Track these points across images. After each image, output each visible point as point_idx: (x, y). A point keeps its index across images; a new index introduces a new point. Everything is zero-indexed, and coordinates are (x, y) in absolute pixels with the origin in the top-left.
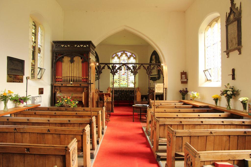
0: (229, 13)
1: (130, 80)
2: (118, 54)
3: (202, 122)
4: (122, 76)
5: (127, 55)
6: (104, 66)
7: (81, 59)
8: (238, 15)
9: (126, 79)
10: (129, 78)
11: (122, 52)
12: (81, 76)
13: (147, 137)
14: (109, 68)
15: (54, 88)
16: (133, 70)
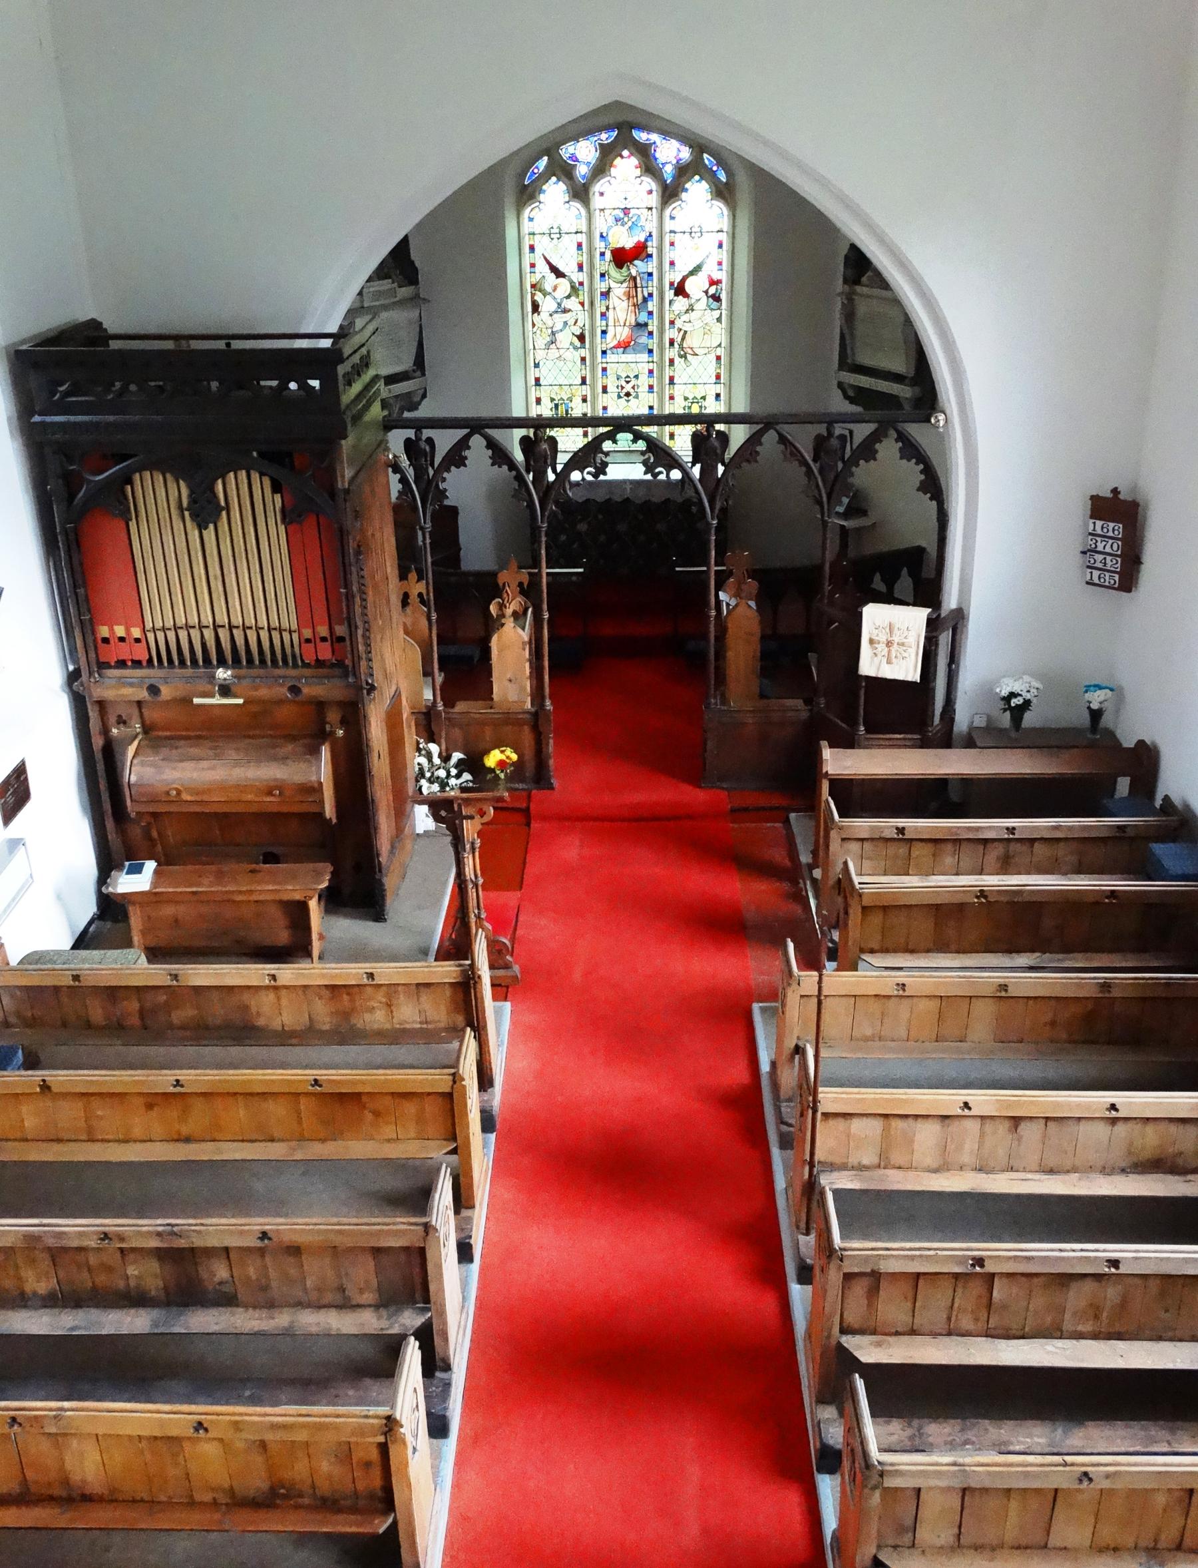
1: (678, 391)
2: (566, 151)
3: (1115, 1263)
4: (610, 357)
5: (650, 167)
6: (463, 444)
7: (276, 488)
9: (644, 381)
11: (606, 137)
12: (290, 620)
14: (500, 455)
15: (93, 714)
16: (696, 471)
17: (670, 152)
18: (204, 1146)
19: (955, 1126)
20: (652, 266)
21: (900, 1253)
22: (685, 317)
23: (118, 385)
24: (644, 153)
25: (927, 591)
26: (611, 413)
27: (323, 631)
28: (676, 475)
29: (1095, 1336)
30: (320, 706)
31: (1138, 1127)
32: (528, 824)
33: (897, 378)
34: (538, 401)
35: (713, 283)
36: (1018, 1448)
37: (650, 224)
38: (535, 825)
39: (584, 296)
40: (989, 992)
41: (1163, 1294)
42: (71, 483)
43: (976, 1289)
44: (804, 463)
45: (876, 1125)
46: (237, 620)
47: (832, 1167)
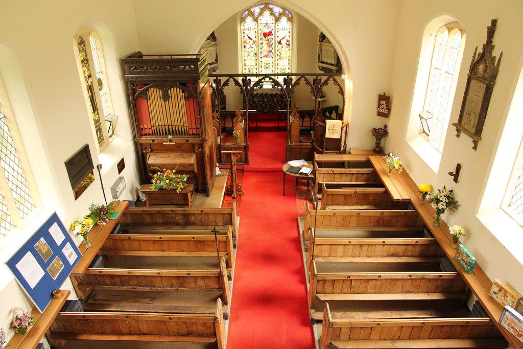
0: (479, 54)
1: (279, 67)
2: (253, 9)
3: (380, 276)
5: (272, 14)
6: (228, 80)
7: (183, 92)
8: (490, 75)
10: (277, 63)
11: (262, 6)
13: (304, 253)
14: (237, 83)
16: (285, 87)
17: (277, 10)
18: (167, 252)
19: (346, 247)
20: (273, 37)
21: (330, 275)
22: (281, 49)
23: (145, 67)
24: (271, 10)
25: (340, 117)
26: (263, 73)
27: (194, 126)
28: (280, 88)
29: (375, 293)
30: (193, 145)
31: (389, 246)
32: (243, 173)
33: (332, 65)
34: (245, 69)
35: (288, 41)
36: (357, 318)
37: (273, 27)
38: (245, 173)
39: (256, 44)
40: (356, 215)
41: (390, 283)
42: (134, 91)
43: (348, 283)
44: (311, 86)
45: (329, 247)
46: (173, 124)
47: (317, 257)
